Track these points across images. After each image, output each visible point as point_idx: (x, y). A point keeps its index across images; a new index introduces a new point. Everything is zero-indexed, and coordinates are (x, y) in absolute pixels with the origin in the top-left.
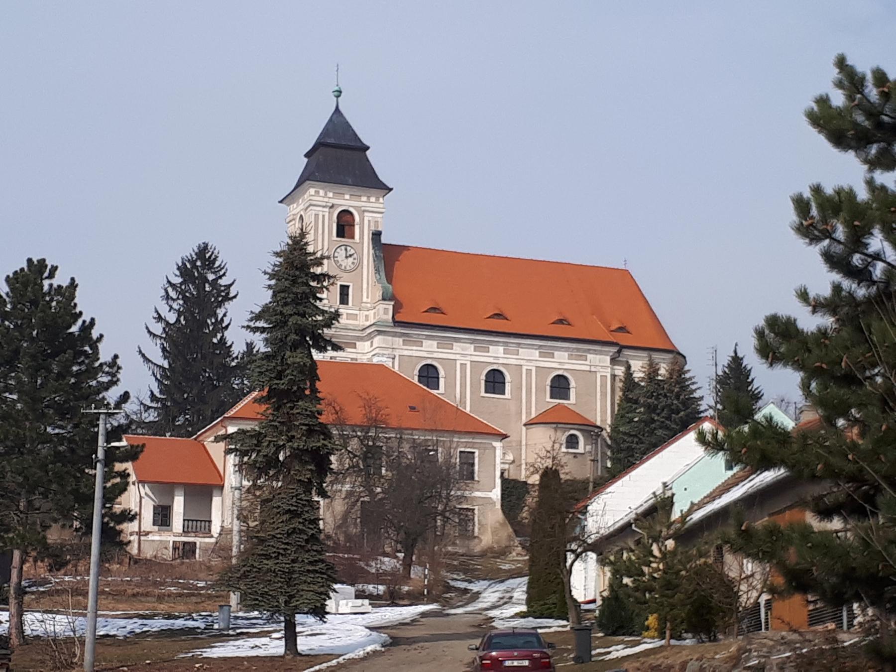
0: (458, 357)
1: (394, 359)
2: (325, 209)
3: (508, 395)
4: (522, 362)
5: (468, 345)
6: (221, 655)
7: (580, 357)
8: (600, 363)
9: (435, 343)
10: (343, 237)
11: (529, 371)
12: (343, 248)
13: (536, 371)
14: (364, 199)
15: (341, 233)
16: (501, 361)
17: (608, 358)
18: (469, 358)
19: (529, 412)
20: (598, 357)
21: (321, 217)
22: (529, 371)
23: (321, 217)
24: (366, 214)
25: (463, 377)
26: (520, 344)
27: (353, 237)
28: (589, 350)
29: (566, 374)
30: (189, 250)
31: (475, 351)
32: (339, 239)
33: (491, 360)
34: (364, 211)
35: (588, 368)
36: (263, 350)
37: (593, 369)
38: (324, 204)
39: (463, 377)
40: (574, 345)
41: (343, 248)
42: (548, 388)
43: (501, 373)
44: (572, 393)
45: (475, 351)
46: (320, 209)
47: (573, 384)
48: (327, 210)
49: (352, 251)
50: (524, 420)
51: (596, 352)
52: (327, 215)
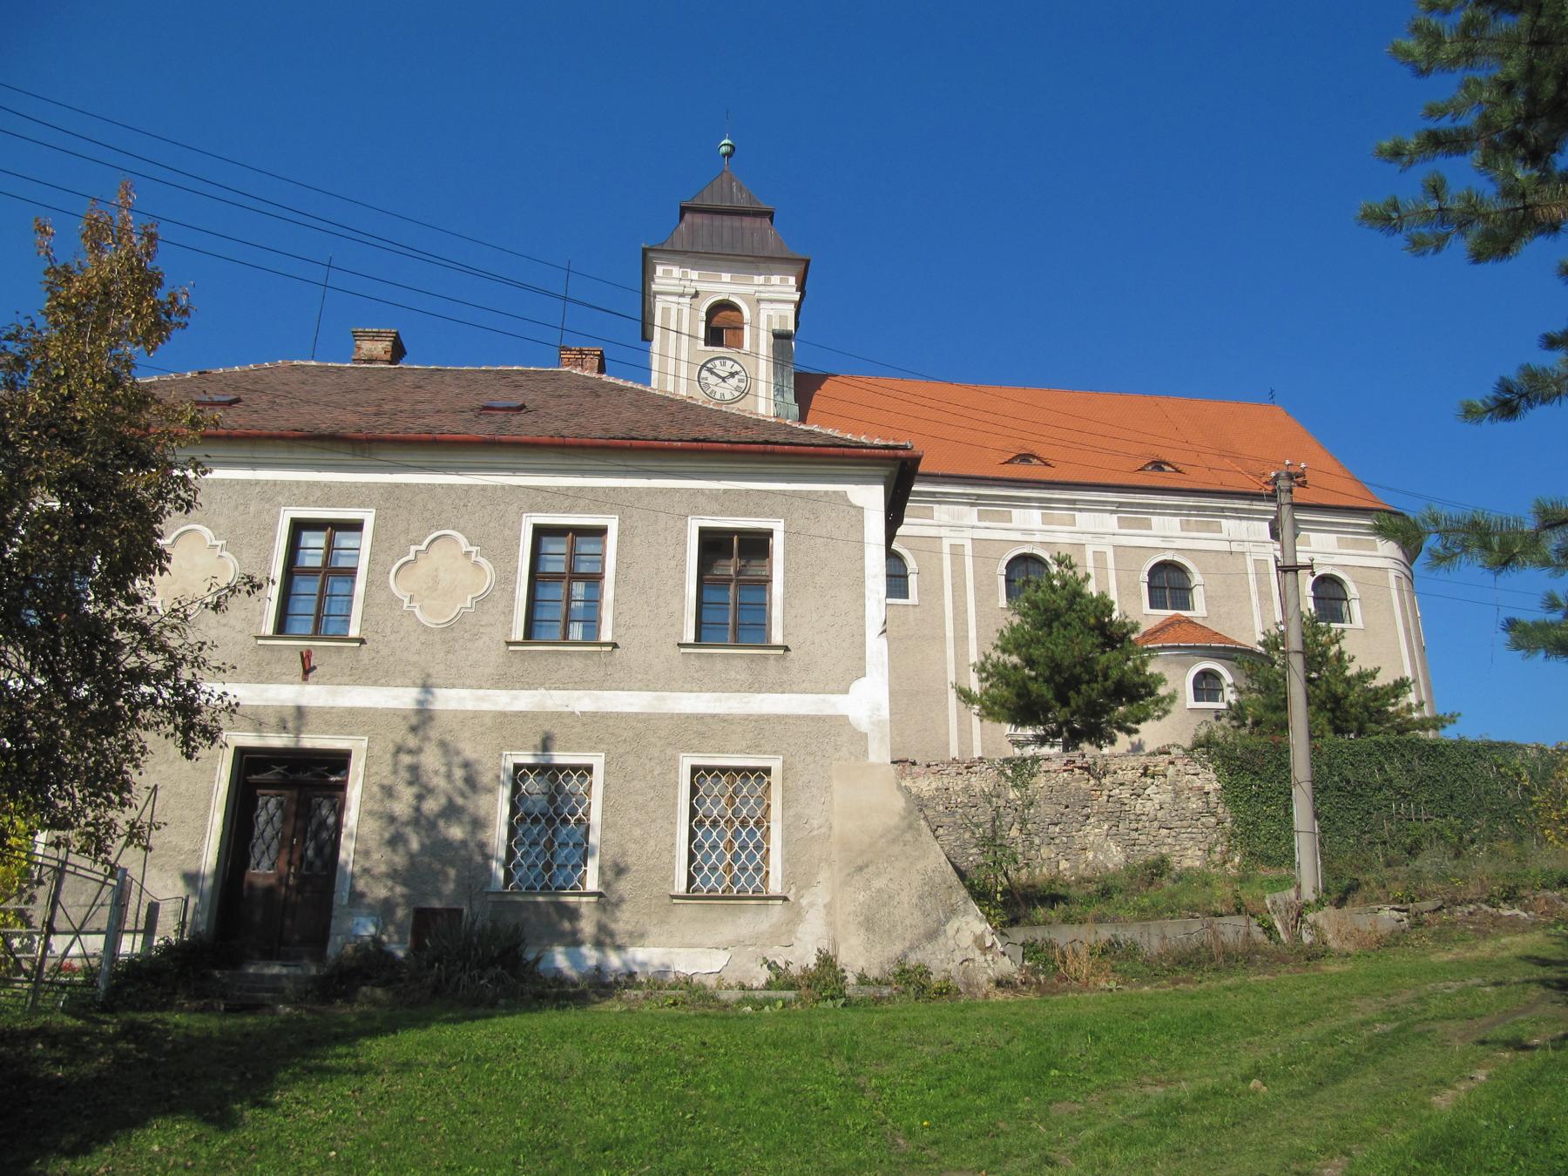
0: (943, 532)
2: (682, 300)
4: (1083, 539)
5: (967, 508)
6: (689, 710)
7: (1207, 527)
8: (1246, 536)
10: (721, 344)
14: (759, 279)
15: (714, 336)
16: (1038, 538)
18: (969, 533)
20: (1244, 523)
21: (674, 313)
23: (674, 313)
24: (763, 305)
25: (958, 573)
26: (1074, 502)
27: (740, 345)
28: (1222, 509)
30: (1488, 267)
31: (980, 519)
32: (710, 348)
34: (758, 301)
35: (1225, 546)
36: (149, 737)
37: (1235, 547)
38: (680, 290)
39: (958, 573)
41: (705, 373)
42: (1145, 587)
44: (1198, 596)
45: (980, 519)
46: (674, 299)
47: (1196, 578)
48: (687, 300)
49: (737, 368)
51: (1238, 514)
52: (686, 311)
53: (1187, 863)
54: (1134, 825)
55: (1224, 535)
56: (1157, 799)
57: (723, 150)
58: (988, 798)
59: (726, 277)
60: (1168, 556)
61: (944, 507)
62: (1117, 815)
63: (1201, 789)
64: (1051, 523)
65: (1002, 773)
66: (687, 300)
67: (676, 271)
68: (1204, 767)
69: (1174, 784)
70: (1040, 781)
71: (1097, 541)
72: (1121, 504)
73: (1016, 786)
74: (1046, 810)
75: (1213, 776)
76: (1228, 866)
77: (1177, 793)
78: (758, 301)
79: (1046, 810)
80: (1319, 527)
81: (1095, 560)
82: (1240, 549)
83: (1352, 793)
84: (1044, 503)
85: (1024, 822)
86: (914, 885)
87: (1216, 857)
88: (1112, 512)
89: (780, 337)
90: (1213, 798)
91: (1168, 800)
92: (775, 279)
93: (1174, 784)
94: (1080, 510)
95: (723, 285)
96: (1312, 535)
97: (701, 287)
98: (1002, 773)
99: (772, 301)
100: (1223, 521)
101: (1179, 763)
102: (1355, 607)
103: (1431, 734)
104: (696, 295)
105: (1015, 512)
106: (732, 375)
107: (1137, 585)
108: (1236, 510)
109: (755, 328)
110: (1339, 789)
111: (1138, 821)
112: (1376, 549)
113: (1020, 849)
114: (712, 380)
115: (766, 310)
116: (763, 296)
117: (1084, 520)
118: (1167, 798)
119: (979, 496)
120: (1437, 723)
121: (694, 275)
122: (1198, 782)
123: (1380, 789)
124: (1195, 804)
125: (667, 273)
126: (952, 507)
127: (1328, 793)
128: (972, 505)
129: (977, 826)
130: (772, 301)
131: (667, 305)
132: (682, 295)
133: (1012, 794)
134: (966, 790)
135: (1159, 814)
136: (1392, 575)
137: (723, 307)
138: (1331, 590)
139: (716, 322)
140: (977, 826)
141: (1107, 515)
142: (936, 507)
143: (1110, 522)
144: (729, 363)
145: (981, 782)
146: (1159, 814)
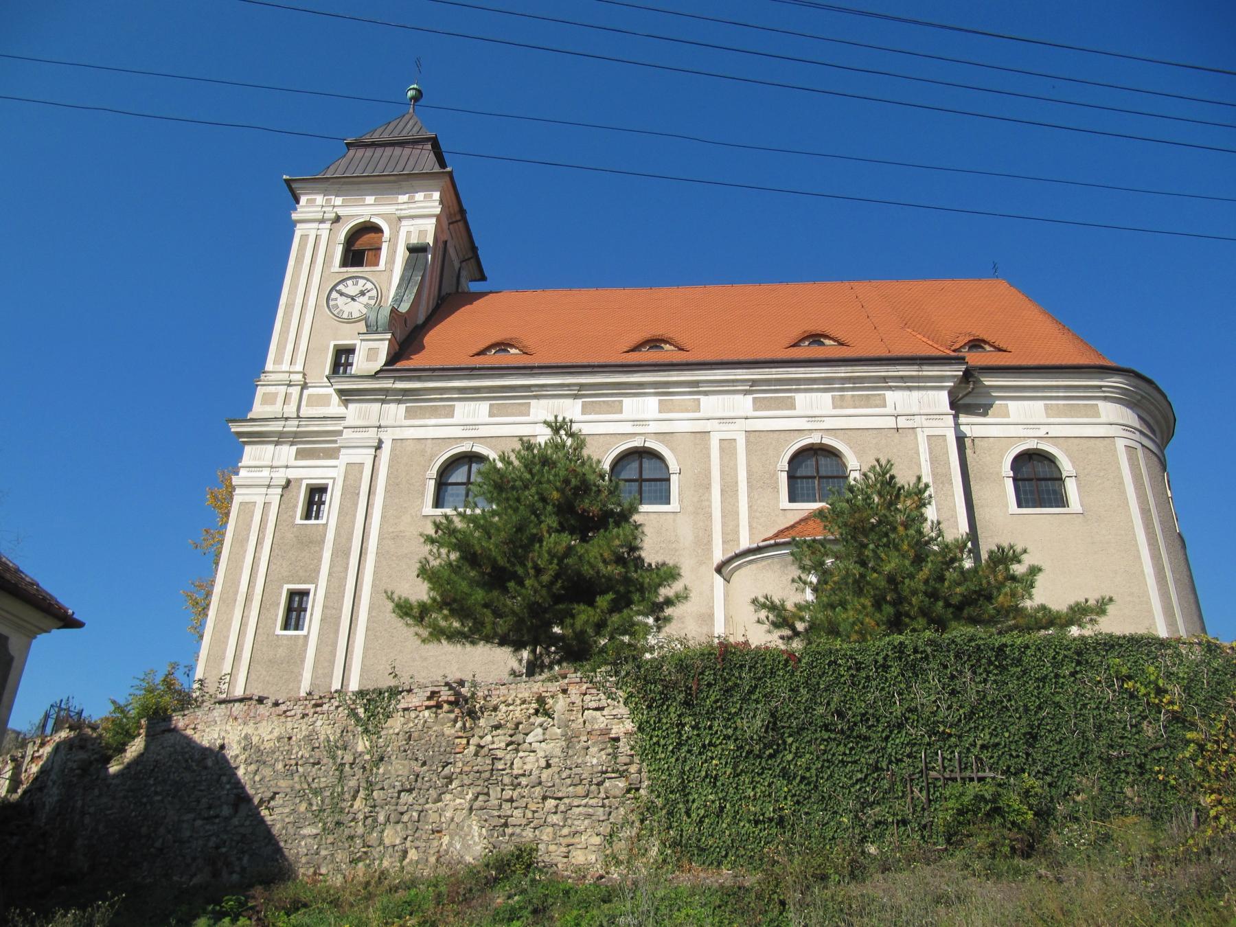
1: (378, 447)
2: (322, 226)
3: (674, 505)
4: (707, 426)
9: (484, 407)
11: (727, 446)
12: (334, 295)
13: (747, 441)
14: (403, 198)
16: (653, 427)
17: (944, 397)
19: (730, 535)
20: (916, 394)
22: (727, 446)
23: (288, 357)
24: (404, 223)
26: (696, 384)
28: (885, 379)
29: (652, 444)
32: (344, 269)
33: (627, 428)
34: (400, 219)
35: (890, 422)
37: (902, 422)
38: (320, 216)
40: (842, 372)
41: (334, 295)
42: (783, 478)
43: (832, 453)
45: (583, 413)
46: (315, 225)
49: (369, 286)
50: (718, 557)
51: (906, 384)
53: (579, 857)
54: (508, 794)
55: (889, 410)
56: (542, 750)
57: (410, 94)
58: (331, 751)
59: (370, 199)
60: (815, 439)
61: (543, 402)
62: (489, 775)
63: (605, 732)
64: (670, 411)
65: (353, 713)
66: (328, 225)
67: (320, 199)
68: (610, 696)
69: (566, 725)
70: (396, 724)
71: (724, 427)
72: (754, 382)
73: (366, 731)
74: (397, 769)
75: (623, 710)
76: (638, 864)
77: (570, 740)
78: (400, 219)
79: (397, 769)
80: (1020, 394)
81: (722, 449)
82: (910, 424)
83: (847, 735)
84: (661, 389)
85: (370, 786)
86: (1136, 820)
87: (620, 846)
88: (746, 392)
89: (416, 250)
90: (624, 747)
91: (558, 752)
92: (419, 196)
93: (566, 725)
94: (706, 393)
95: (367, 208)
96: (1011, 404)
97: (341, 212)
98: (353, 713)
99: (413, 217)
100: (888, 394)
101: (573, 690)
102: (1071, 487)
103: (1074, 631)
104: (338, 219)
105: (627, 402)
106: (362, 293)
107: (774, 476)
108: (902, 378)
109: (393, 242)
110: (826, 727)
111: (515, 786)
112: (1097, 415)
113: (360, 830)
114: (341, 301)
115: (406, 226)
116: (403, 213)
117: (711, 404)
118: (554, 748)
119: (582, 386)
120: (1079, 613)
121: (338, 201)
122: (600, 720)
123: (900, 726)
124: (596, 758)
125: (311, 202)
126: (551, 401)
127: (807, 736)
128: (576, 397)
129: (316, 792)
130: (413, 217)
131: (305, 232)
132: (322, 221)
133: (362, 744)
134: (309, 738)
135: (544, 776)
136: (1120, 444)
137: (369, 228)
138: (1042, 469)
139: (358, 246)
140: (316, 792)
141: (740, 397)
142: (533, 402)
143: (743, 404)
144: (361, 282)
145: (325, 729)
146: (545, 775)
